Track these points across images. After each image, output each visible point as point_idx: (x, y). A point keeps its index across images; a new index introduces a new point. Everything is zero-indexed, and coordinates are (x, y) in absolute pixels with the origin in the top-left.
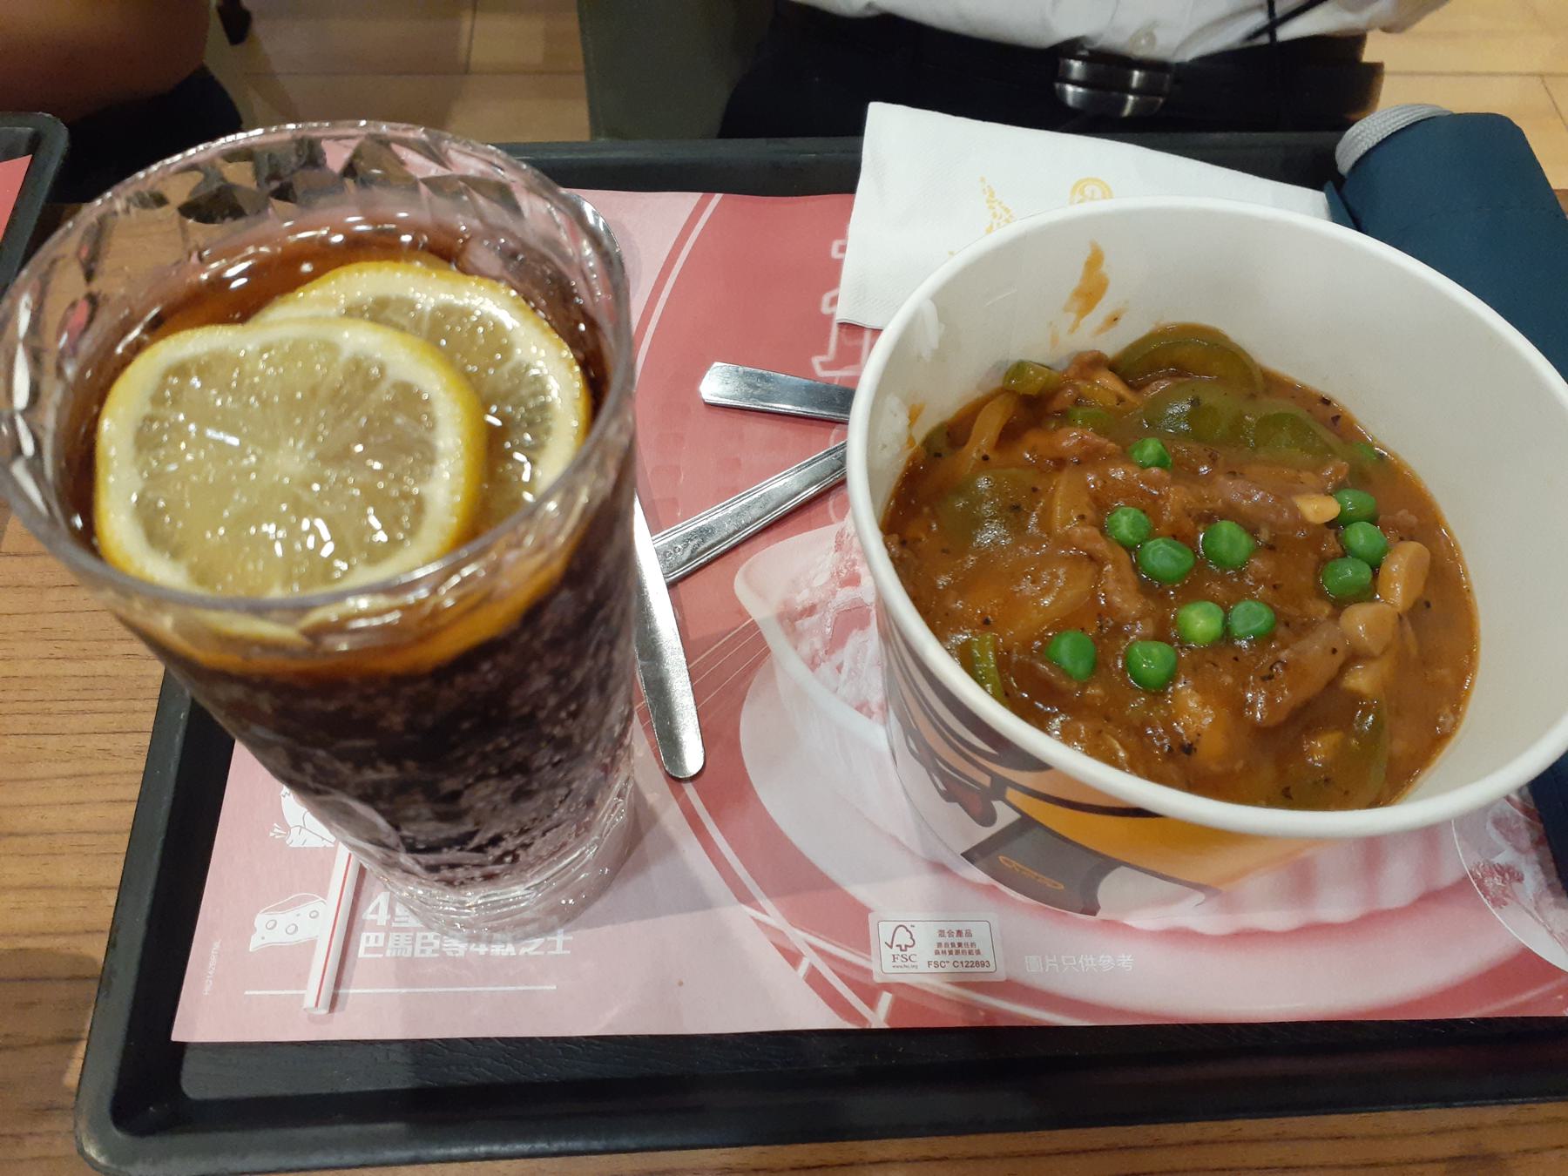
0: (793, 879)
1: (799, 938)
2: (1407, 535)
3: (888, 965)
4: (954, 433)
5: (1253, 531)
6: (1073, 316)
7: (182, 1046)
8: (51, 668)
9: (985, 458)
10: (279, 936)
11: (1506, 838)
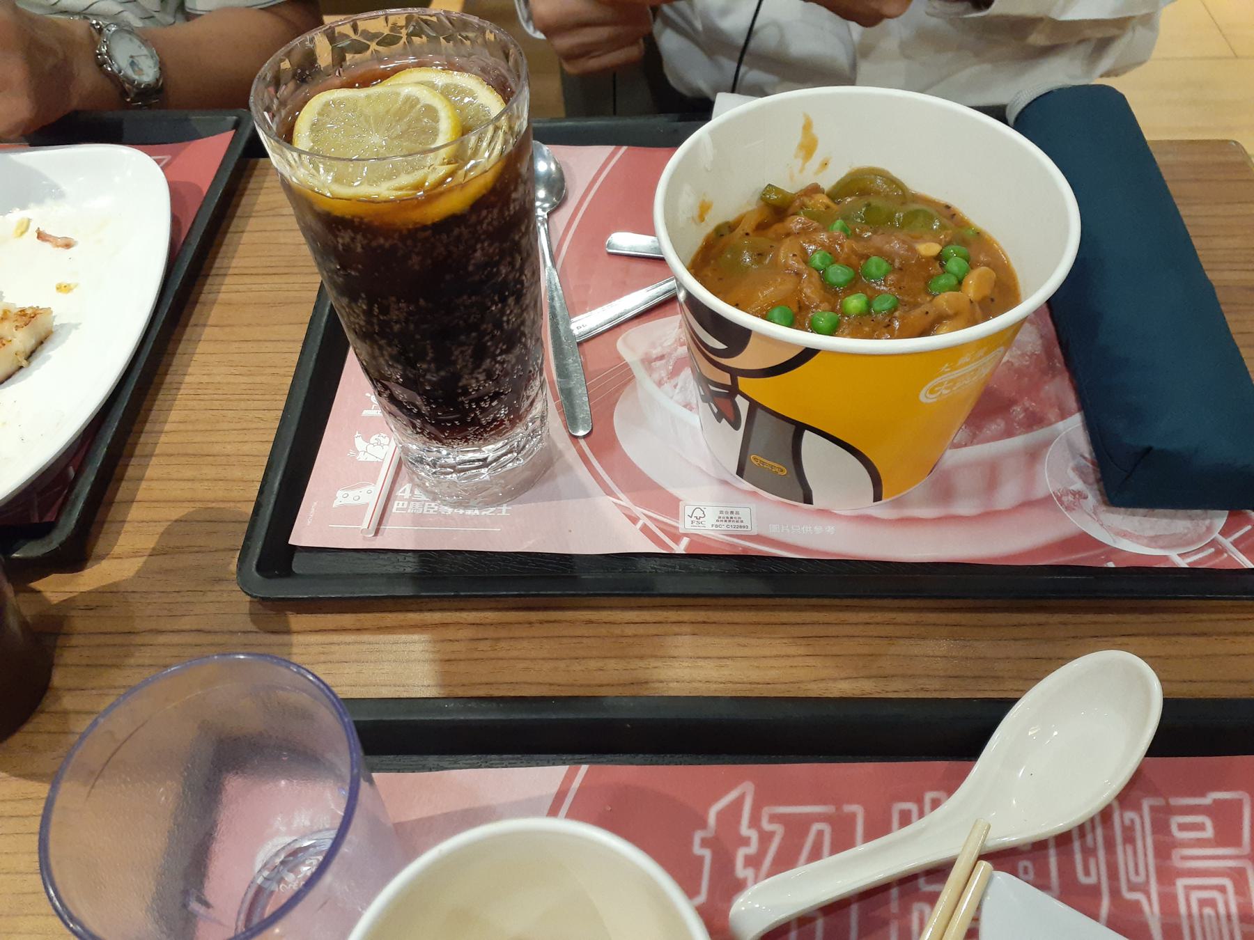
0: (639, 485)
1: (638, 511)
5: (892, 264)
6: (800, 161)
8: (232, 379)
10: (350, 501)
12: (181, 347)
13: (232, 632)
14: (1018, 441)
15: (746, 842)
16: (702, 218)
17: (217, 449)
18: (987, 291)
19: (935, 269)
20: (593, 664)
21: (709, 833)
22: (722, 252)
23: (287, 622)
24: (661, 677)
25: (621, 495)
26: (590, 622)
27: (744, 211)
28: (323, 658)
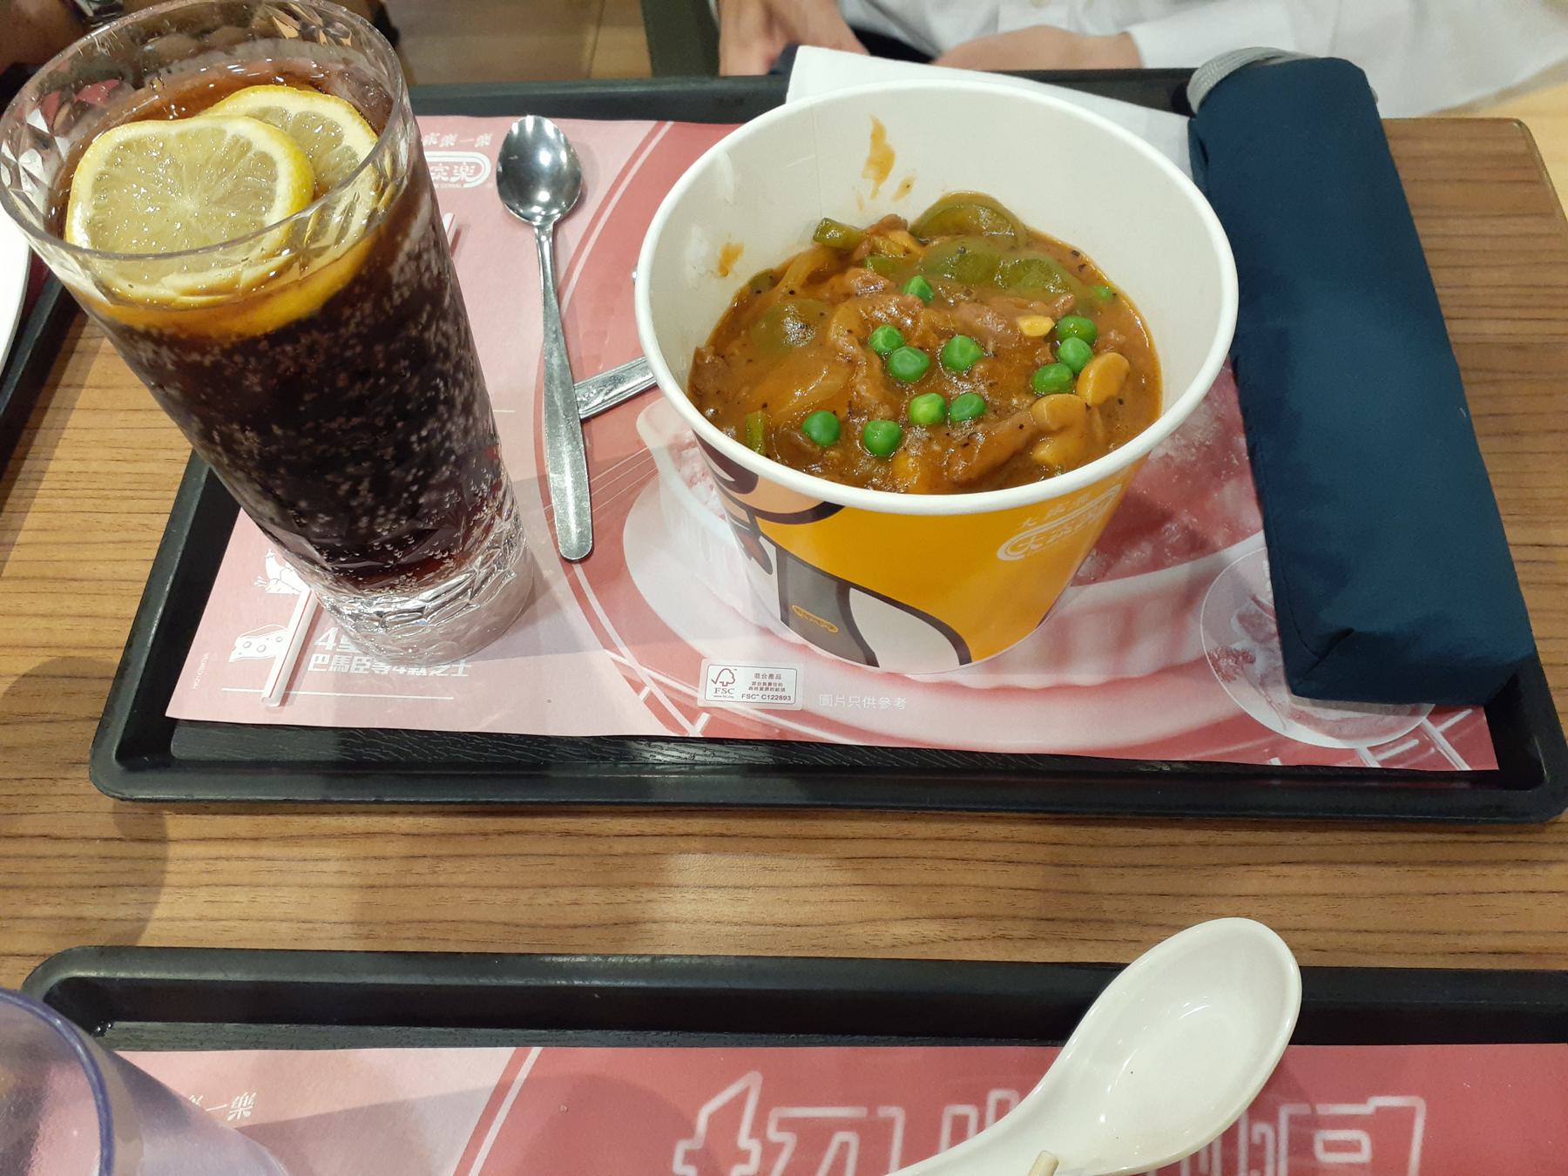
0: (650, 634)
1: (644, 673)
3: (710, 695)
4: (771, 279)
5: (983, 345)
6: (870, 183)
7: (174, 722)
8: (113, 466)
9: (792, 293)
10: (251, 653)
11: (1247, 629)
12: (48, 419)
13: (87, 839)
14: (1178, 573)
15: (744, 1157)
16: (724, 270)
17: (84, 570)
18: (1112, 389)
19: (1043, 353)
20: (566, 895)
21: (696, 1143)
22: (756, 319)
23: (162, 826)
24: (658, 915)
25: (624, 649)
26: (568, 834)
27: (795, 253)
28: (206, 878)
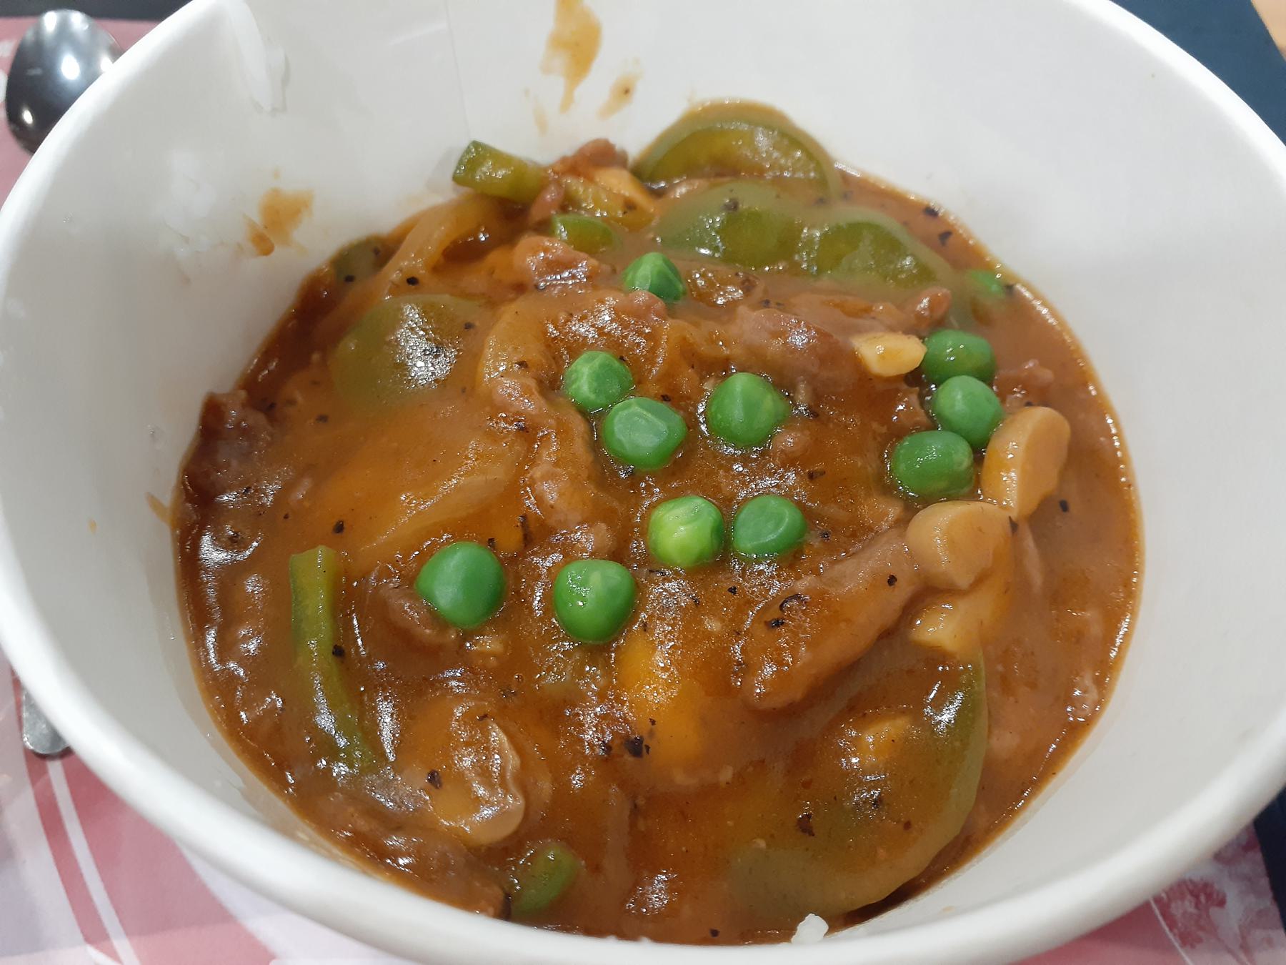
2: (1039, 396)
9: (412, 281)
